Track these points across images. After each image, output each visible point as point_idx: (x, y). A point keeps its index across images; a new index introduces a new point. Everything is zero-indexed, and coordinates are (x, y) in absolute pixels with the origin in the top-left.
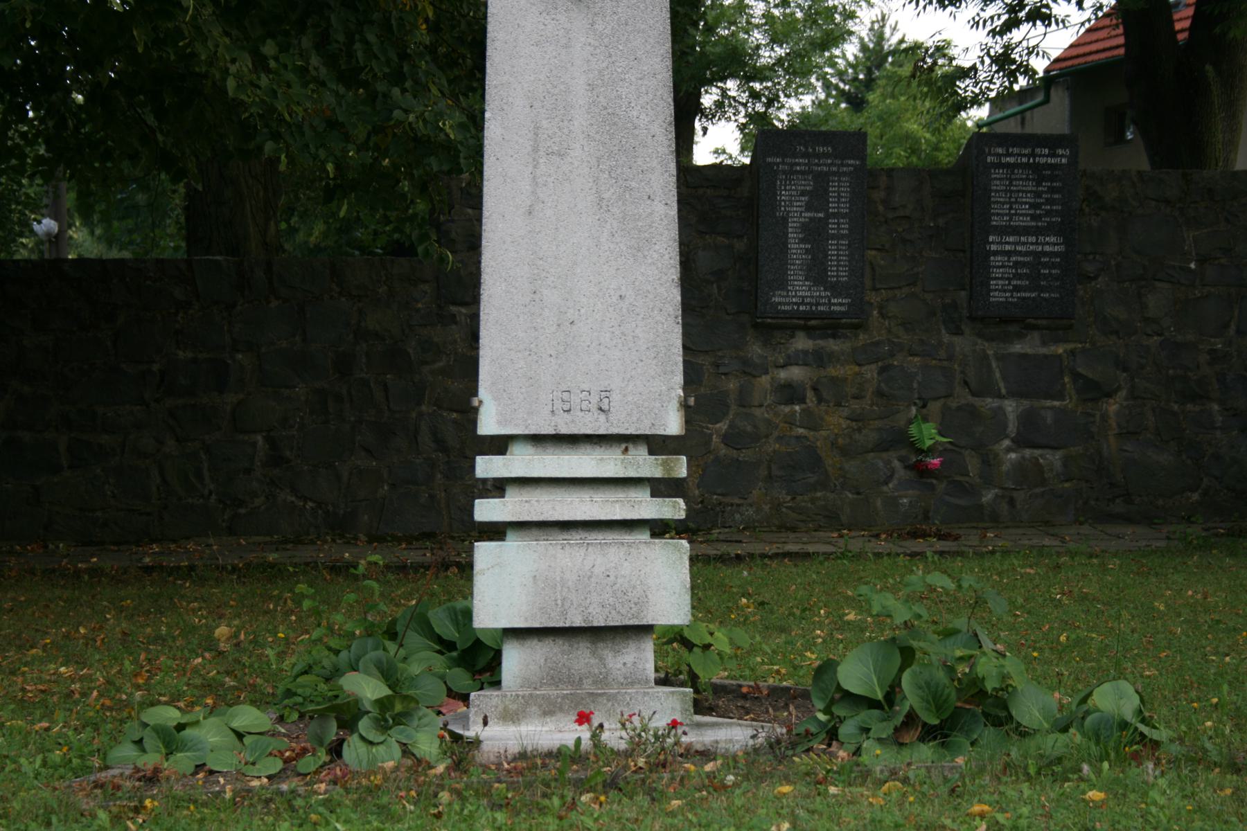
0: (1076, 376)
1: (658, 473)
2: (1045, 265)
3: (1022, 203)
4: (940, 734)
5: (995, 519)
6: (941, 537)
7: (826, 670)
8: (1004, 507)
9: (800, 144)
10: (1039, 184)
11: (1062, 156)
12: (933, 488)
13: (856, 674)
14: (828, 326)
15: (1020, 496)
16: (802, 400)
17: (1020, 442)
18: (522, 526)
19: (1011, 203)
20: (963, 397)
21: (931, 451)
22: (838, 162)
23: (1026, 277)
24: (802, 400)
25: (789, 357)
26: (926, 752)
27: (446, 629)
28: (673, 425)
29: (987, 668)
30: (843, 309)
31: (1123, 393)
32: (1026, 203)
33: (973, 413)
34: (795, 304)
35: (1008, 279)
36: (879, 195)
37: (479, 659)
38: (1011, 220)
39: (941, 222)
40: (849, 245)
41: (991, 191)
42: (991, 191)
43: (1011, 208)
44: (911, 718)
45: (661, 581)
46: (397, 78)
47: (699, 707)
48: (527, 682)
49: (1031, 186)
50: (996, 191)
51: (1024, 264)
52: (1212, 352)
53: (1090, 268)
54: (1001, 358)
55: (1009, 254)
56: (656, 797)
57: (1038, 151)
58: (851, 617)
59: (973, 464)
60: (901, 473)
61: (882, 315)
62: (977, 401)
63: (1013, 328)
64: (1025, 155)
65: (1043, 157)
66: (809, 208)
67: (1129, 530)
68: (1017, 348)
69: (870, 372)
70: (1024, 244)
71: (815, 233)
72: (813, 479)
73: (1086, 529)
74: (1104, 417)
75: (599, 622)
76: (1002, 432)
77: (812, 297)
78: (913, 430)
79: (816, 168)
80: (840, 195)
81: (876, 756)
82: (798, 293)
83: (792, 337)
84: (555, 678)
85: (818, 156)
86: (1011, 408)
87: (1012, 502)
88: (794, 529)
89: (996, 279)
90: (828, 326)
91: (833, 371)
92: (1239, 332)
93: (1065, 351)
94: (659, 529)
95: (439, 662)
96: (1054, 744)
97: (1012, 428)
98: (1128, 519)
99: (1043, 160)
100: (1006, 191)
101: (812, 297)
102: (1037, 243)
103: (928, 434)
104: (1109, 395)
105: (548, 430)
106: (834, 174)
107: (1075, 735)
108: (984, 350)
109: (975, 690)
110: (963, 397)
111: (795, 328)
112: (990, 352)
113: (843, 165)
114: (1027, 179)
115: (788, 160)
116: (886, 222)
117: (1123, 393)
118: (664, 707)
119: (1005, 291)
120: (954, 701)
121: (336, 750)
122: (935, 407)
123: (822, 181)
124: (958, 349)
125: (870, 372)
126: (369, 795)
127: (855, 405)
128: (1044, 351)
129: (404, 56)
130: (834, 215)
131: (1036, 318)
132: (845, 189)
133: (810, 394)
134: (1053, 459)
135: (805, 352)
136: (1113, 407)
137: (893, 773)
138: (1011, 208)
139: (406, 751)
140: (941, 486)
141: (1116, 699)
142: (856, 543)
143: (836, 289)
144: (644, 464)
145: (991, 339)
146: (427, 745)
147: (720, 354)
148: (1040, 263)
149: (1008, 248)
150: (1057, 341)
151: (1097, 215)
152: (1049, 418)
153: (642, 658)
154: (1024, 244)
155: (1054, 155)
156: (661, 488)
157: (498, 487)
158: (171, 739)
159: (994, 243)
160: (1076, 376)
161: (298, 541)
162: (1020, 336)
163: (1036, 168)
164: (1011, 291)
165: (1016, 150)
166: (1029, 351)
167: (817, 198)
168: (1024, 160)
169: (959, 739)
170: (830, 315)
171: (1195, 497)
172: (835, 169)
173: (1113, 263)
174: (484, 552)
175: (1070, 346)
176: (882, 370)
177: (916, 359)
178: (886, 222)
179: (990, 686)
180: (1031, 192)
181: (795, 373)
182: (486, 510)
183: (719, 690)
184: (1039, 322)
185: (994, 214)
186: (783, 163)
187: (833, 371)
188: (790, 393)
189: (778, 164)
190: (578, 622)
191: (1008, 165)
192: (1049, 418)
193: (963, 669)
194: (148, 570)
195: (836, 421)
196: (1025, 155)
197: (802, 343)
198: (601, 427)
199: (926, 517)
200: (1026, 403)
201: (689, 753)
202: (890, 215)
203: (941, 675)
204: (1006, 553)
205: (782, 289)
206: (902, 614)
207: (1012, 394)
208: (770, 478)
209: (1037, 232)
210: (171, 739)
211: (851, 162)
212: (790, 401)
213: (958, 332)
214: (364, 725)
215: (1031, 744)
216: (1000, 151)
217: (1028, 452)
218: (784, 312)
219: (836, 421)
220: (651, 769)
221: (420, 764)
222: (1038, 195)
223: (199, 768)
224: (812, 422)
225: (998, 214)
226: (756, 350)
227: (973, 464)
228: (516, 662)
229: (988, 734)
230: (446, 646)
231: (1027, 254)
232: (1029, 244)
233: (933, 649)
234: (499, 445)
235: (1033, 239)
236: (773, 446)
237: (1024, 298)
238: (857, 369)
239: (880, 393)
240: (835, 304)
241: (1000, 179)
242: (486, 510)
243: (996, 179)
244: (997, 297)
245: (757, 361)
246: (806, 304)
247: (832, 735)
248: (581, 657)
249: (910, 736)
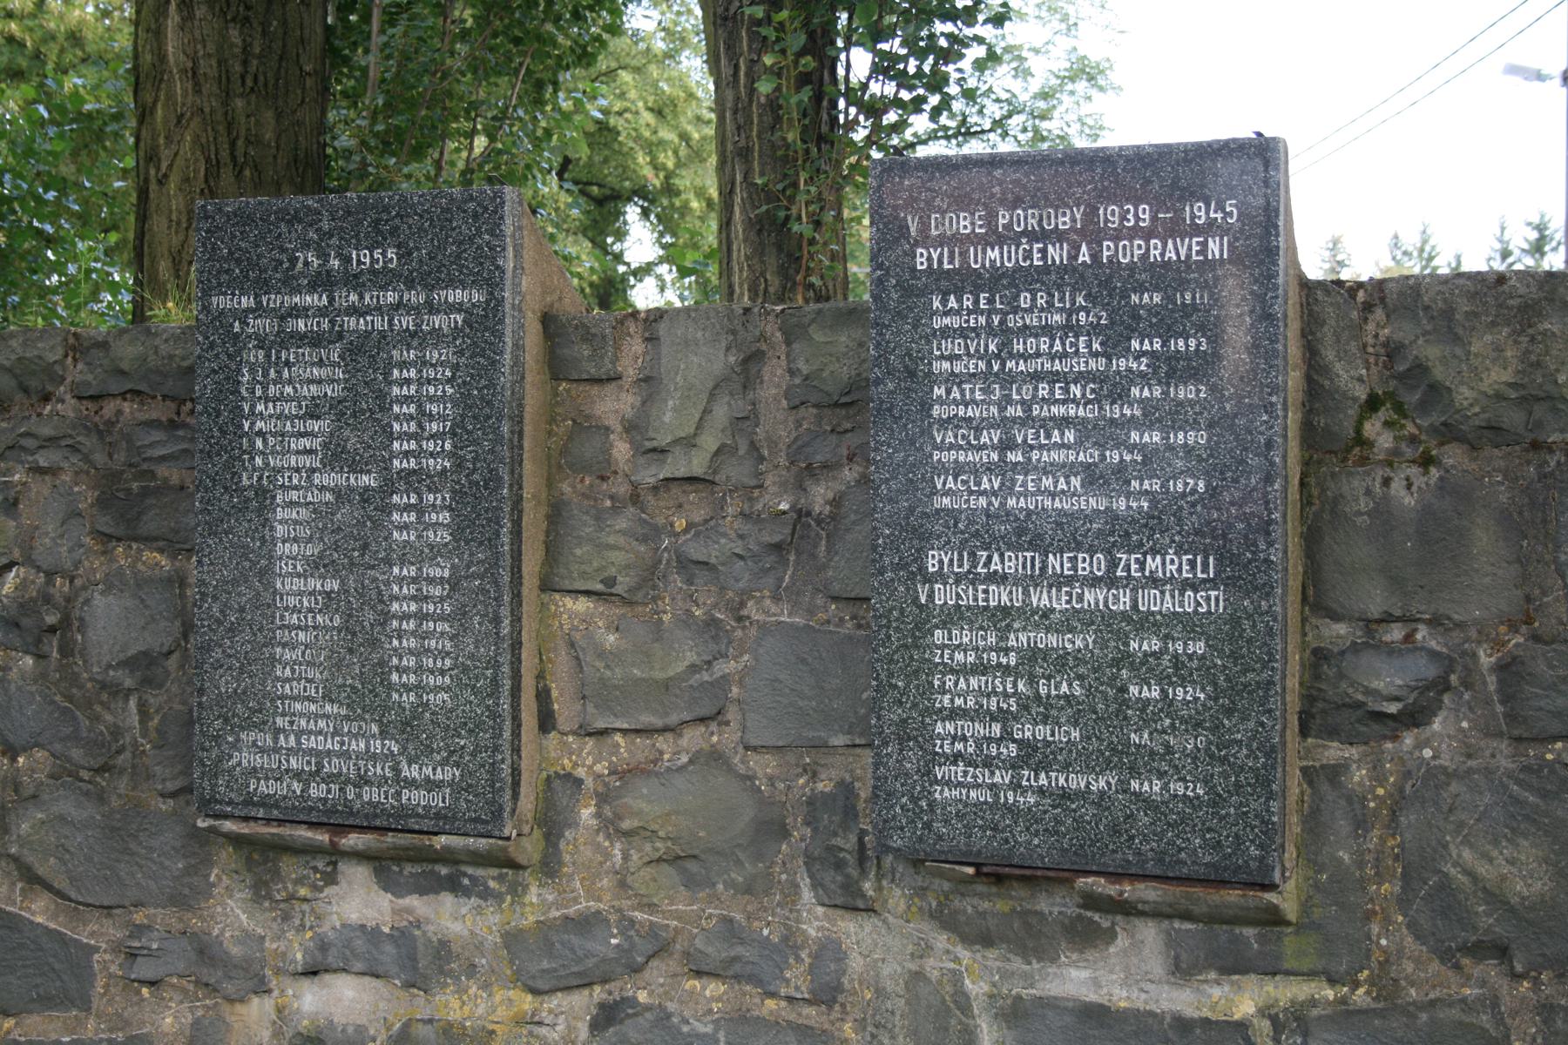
2: (1145, 668)
3: (1046, 425)
9: (306, 246)
10: (1114, 345)
11: (1210, 228)
19: (1004, 423)
22: (415, 297)
23: (1077, 711)
25: (323, 946)
30: (438, 801)
32: (1063, 423)
34: (298, 775)
35: (1002, 716)
36: (613, 406)
38: (1007, 489)
39: (819, 496)
40: (454, 584)
41: (931, 379)
42: (931, 379)
43: (1007, 445)
49: (1085, 358)
50: (953, 379)
51: (1062, 662)
55: (1001, 617)
57: (1110, 214)
61: (610, 826)
63: (1053, 905)
64: (1059, 236)
68: (1074, 979)
70: (1060, 581)
77: (345, 755)
79: (351, 323)
82: (304, 738)
83: (331, 879)
85: (353, 281)
89: (954, 714)
93: (1262, 1012)
99: (1130, 252)
100: (986, 376)
101: (345, 755)
102: (1110, 581)
106: (411, 337)
108: (956, 978)
112: (976, 988)
113: (432, 308)
114: (1069, 328)
115: (273, 300)
116: (635, 499)
119: (988, 763)
124: (856, 963)
128: (1180, 1000)
130: (412, 479)
131: (1115, 876)
135: (372, 934)
138: (1007, 445)
147: (139, 917)
148: (1123, 659)
149: (1000, 596)
150: (1234, 965)
151: (1426, 461)
154: (1060, 581)
155: (1176, 229)
162: (1084, 937)
163: (1105, 284)
164: (1014, 765)
165: (1025, 218)
166: (1121, 996)
167: (358, 416)
168: (1057, 254)
172: (407, 322)
173: (1486, 659)
175: (1287, 992)
177: (714, 988)
178: (635, 499)
180: (1081, 378)
184: (1128, 890)
185: (942, 469)
186: (259, 310)
189: (243, 315)
191: (996, 280)
196: (1059, 236)
197: (358, 901)
202: (649, 475)
205: (260, 726)
209: (1119, 534)
211: (456, 295)
213: (852, 903)
216: (963, 224)
218: (266, 802)
222: (1113, 388)
225: (958, 470)
226: (233, 914)
231: (1072, 621)
232: (1079, 589)
235: (1097, 564)
237: (1065, 795)
238: (527, 1002)
240: (412, 784)
241: (963, 333)
243: (946, 332)
245: (235, 951)
246: (330, 779)
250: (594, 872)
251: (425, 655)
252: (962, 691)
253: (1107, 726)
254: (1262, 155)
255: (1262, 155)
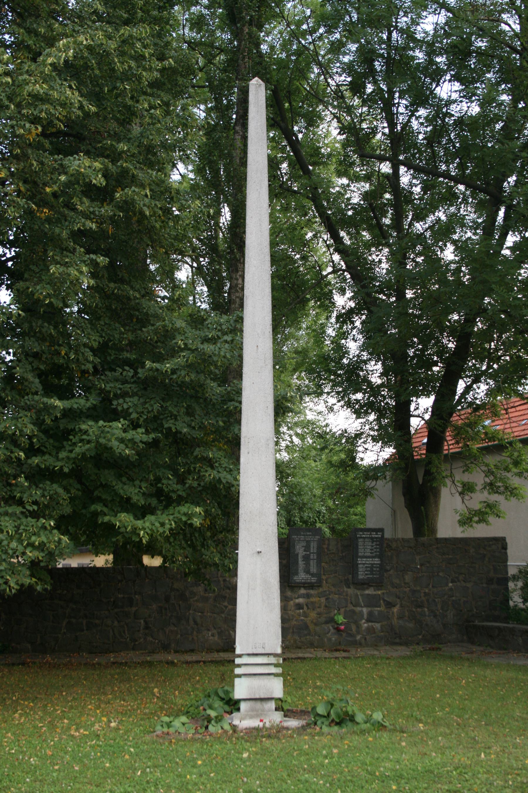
0: (384, 600)
1: (276, 662)
4: (339, 724)
5: (360, 644)
6: (344, 651)
7: (314, 708)
8: (363, 641)
12: (341, 635)
13: (321, 710)
14: (310, 586)
15: (368, 637)
16: (303, 608)
17: (368, 621)
18: (245, 675)
20: (351, 607)
21: (341, 624)
24: (303, 608)
26: (336, 728)
27: (222, 695)
28: (279, 651)
29: (349, 709)
31: (398, 606)
33: (354, 612)
36: (325, 546)
37: (233, 705)
44: (333, 721)
45: (276, 688)
46: (203, 545)
47: (285, 716)
48: (246, 711)
49: (370, 544)
52: (425, 593)
53: (388, 568)
54: (361, 595)
56: (279, 738)
58: (318, 684)
59: (354, 628)
60: (332, 630)
62: (355, 608)
63: (365, 586)
65: (374, 535)
66: (305, 551)
67: (399, 648)
68: (367, 592)
69: (323, 600)
71: (306, 558)
72: (306, 632)
73: (387, 648)
74: (393, 613)
75: (262, 697)
76: (362, 617)
78: (336, 618)
80: (314, 547)
81: (325, 729)
84: (252, 710)
86: (365, 610)
87: (365, 639)
88: (300, 648)
90: (310, 586)
91: (312, 600)
92: (433, 587)
94: (276, 675)
95: (221, 703)
96: (364, 726)
97: (365, 616)
98: (400, 644)
103: (340, 619)
104: (394, 606)
105: (251, 652)
107: (368, 725)
109: (346, 713)
110: (351, 607)
111: (300, 587)
117: (398, 606)
118: (277, 717)
120: (342, 716)
121: (207, 728)
122: (342, 610)
123: (308, 542)
125: (323, 600)
126: (218, 739)
127: (318, 610)
128: (375, 593)
129: (204, 540)
132: (315, 545)
133: (305, 607)
134: (377, 626)
136: (395, 610)
137: (329, 734)
139: (222, 728)
140: (344, 635)
141: (378, 716)
142: (320, 653)
143: (313, 575)
144: (273, 660)
145: (359, 589)
146: (227, 727)
150: (378, 590)
152: (376, 613)
153: (272, 705)
156: (276, 665)
157: (239, 666)
158: (169, 725)
159: (359, 561)
160: (384, 600)
161: (153, 652)
162: (367, 588)
163: (372, 538)
167: (307, 548)
169: (343, 725)
170: (311, 583)
171: (420, 637)
174: (237, 681)
176: (327, 599)
179: (350, 713)
181: (301, 600)
182: (237, 671)
183: (288, 710)
187: (312, 600)
188: (299, 606)
190: (258, 697)
192: (376, 613)
193: (344, 709)
194: (114, 663)
195: (313, 615)
197: (303, 591)
198: (263, 652)
199: (340, 644)
200: (369, 609)
201: (284, 728)
203: (339, 710)
204: (363, 658)
206: (331, 696)
207: (366, 606)
208: (293, 632)
210: (169, 725)
212: (299, 609)
213: (349, 587)
214: (213, 722)
215: (359, 727)
217: (370, 624)
219: (313, 615)
220: (276, 733)
221: (226, 732)
223: (176, 731)
224: (306, 615)
227: (354, 628)
228: (243, 706)
229: (350, 724)
230: (222, 699)
232: (370, 561)
233: (338, 705)
234: (240, 656)
236: (294, 622)
239: (326, 606)
242: (237, 671)
244: (360, 577)
247: (315, 724)
248: (258, 705)
249: (333, 725)
250: (325, 587)
251: (313, 569)
252: (360, 570)
253: (372, 571)
254: (503, 539)
255: (503, 539)
